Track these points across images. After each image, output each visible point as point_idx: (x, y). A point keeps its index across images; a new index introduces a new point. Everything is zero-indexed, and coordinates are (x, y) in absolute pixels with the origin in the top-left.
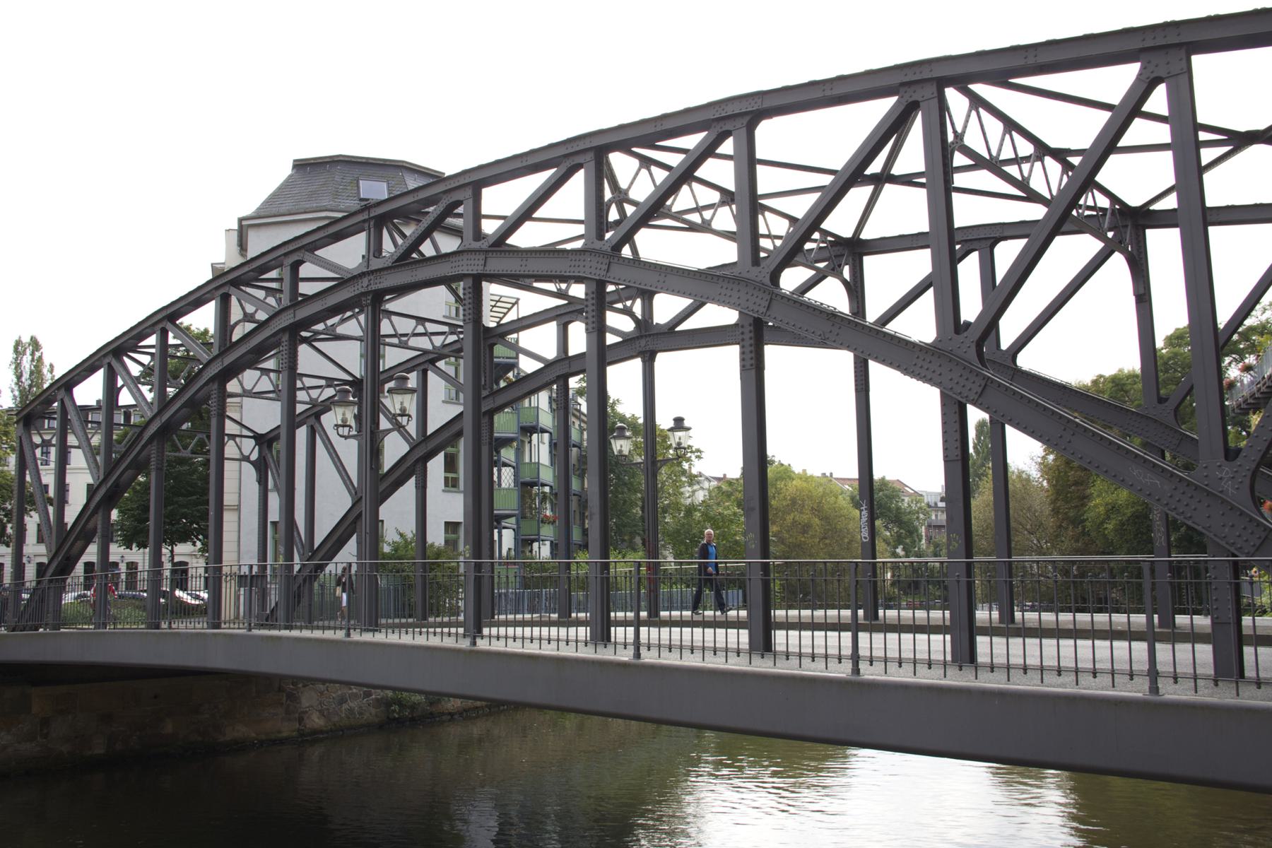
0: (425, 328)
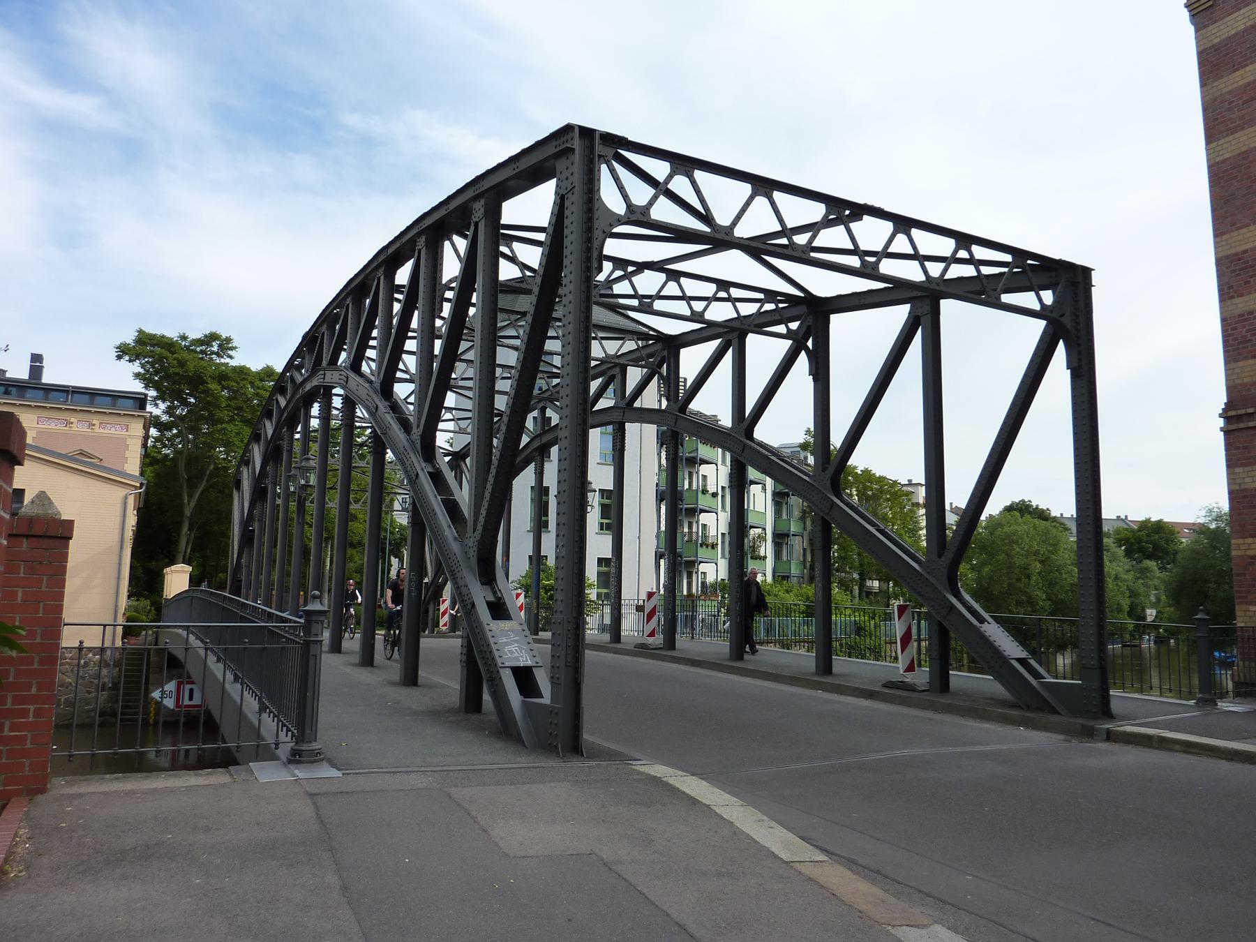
0: (691, 308)
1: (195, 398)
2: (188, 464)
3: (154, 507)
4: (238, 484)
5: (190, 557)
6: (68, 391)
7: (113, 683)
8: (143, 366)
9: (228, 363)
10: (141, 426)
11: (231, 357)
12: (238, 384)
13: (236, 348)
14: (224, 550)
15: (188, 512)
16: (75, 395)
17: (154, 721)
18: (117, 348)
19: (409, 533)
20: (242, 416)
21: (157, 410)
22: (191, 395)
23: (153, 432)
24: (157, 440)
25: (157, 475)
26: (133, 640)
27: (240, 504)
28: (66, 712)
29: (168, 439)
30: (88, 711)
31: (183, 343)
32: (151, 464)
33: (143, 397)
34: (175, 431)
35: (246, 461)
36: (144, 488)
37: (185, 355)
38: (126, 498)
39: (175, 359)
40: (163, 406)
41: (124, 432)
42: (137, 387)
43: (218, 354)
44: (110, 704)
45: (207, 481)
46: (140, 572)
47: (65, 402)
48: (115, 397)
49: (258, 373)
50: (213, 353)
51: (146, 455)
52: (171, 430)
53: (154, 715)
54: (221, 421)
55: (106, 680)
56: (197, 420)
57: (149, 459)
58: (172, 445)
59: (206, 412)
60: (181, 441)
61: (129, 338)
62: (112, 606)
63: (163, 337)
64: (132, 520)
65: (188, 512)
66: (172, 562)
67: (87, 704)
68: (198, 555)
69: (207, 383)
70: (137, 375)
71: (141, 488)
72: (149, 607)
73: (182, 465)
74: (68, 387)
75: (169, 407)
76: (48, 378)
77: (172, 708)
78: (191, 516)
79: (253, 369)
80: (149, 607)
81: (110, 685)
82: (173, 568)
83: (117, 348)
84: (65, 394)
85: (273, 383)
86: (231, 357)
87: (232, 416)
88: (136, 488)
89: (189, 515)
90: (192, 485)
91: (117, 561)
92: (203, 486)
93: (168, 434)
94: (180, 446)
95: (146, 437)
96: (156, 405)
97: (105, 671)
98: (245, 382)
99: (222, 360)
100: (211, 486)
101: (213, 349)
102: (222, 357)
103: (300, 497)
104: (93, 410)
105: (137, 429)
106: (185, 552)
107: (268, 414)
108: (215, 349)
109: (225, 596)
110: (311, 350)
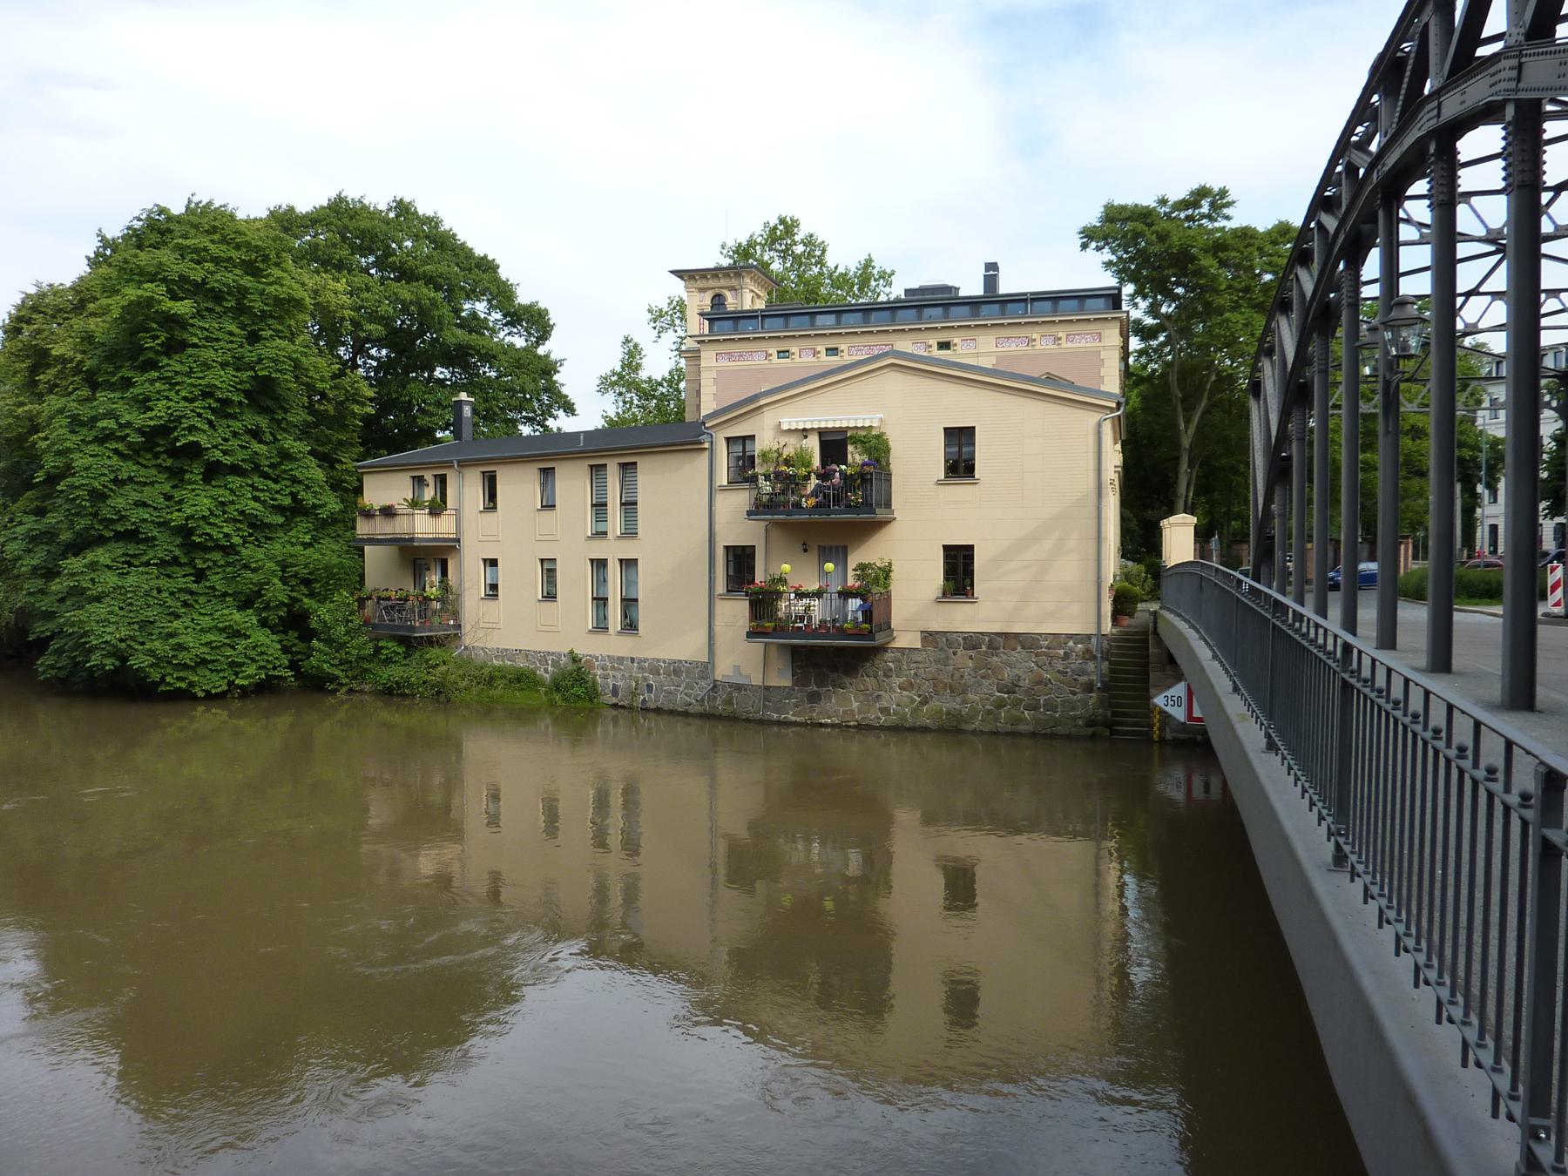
1: (1185, 286)
2: (1182, 380)
3: (1145, 442)
4: (1256, 388)
5: (1193, 503)
6: (1026, 300)
7: (1102, 682)
8: (1113, 252)
9: (1224, 227)
10: (1117, 331)
11: (1228, 218)
12: (1242, 253)
13: (1234, 202)
14: (1241, 492)
15: (1186, 442)
16: (1035, 303)
17: (1160, 737)
18: (1080, 233)
19: (1508, 450)
20: (1250, 299)
21: (1138, 311)
22: (1178, 284)
23: (1135, 343)
24: (1141, 353)
25: (1144, 398)
26: (1126, 621)
27: (1264, 418)
28: (1047, 718)
29: (1155, 351)
30: (1074, 718)
31: (1162, 211)
32: (1136, 385)
33: (1116, 292)
34: (1162, 339)
35: (1267, 348)
36: (1122, 409)
37: (1166, 225)
38: (1099, 425)
39: (1153, 233)
40: (1143, 304)
41: (1097, 344)
42: (1108, 280)
43: (1209, 217)
44: (1101, 710)
45: (1209, 399)
46: (1133, 525)
47: (1024, 315)
48: (1081, 297)
49: (1269, 232)
50: (1203, 216)
51: (1127, 373)
52: (1156, 338)
53: (1159, 729)
54: (1220, 311)
55: (1094, 677)
56: (1190, 317)
57: (1130, 377)
58: (1160, 357)
59: (1202, 306)
60: (1170, 351)
61: (1093, 217)
62: (1092, 577)
63: (1136, 205)
64: (1113, 458)
65: (1186, 442)
66: (1172, 512)
67: (1073, 709)
68: (1203, 499)
69: (1199, 260)
70: (1108, 264)
71: (1118, 409)
72: (1144, 575)
73: (1173, 379)
74: (1026, 294)
75: (1152, 305)
76: (1006, 287)
77: (1183, 720)
78: (1191, 446)
79: (1261, 229)
80: (1144, 575)
81: (1099, 685)
82: (1172, 519)
83: (1080, 233)
84: (1023, 304)
85: (1289, 246)
86: (1228, 218)
87: (1237, 301)
88: (1112, 410)
89: (1187, 447)
90: (1189, 408)
91: (1095, 515)
92: (1203, 405)
93: (1154, 343)
94: (1170, 357)
95: (1125, 354)
96: (1136, 305)
97: (1091, 666)
98: (1250, 249)
99: (1216, 225)
100: (1213, 405)
101: (1202, 211)
102: (1216, 220)
103: (1387, 383)
104: (1057, 319)
105: (1112, 336)
106: (1187, 497)
107: (1284, 306)
108: (1205, 209)
109: (1268, 596)
110: (1390, 92)
